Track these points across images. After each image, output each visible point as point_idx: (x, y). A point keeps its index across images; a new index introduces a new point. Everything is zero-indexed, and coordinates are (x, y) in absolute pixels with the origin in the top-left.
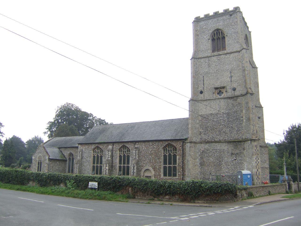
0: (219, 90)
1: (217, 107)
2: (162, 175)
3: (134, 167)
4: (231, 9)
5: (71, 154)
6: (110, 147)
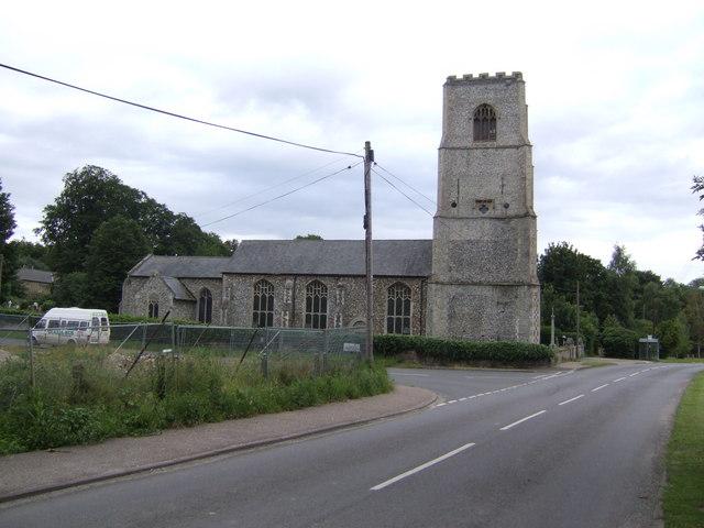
0: (483, 204)
1: (478, 231)
2: (386, 331)
3: (338, 318)
4: (509, 73)
5: (205, 291)
6: (289, 282)
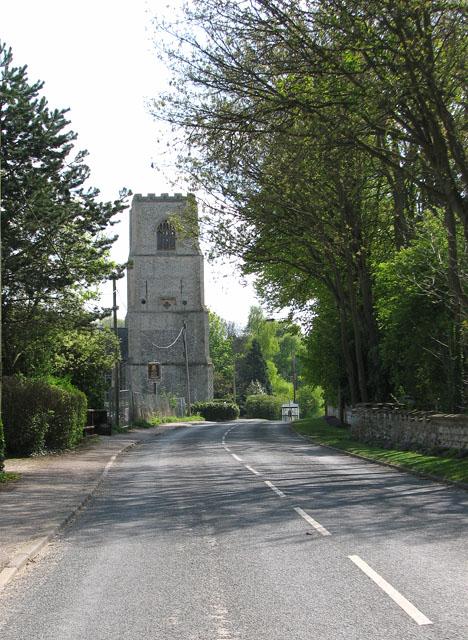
0: (166, 302)
